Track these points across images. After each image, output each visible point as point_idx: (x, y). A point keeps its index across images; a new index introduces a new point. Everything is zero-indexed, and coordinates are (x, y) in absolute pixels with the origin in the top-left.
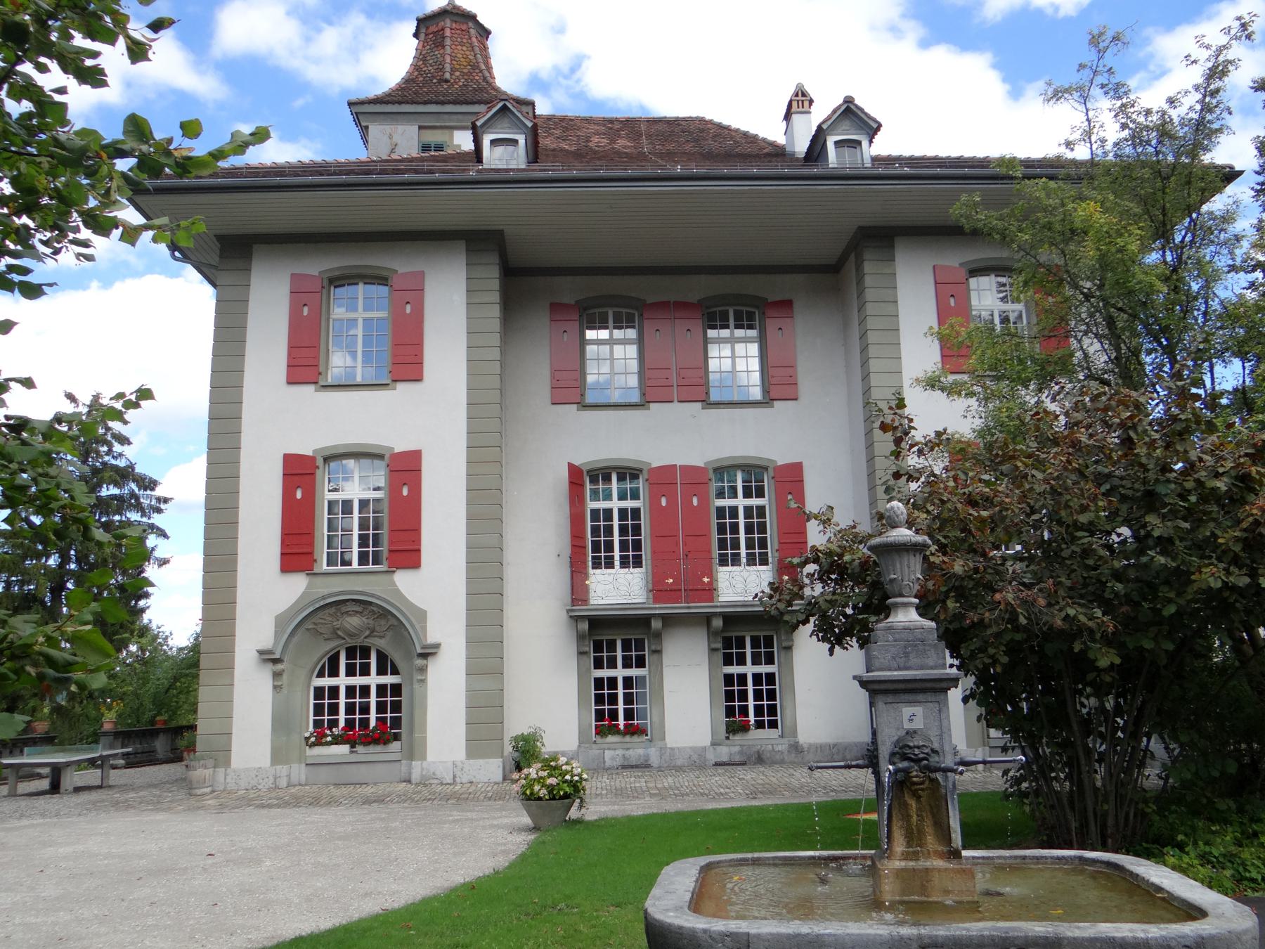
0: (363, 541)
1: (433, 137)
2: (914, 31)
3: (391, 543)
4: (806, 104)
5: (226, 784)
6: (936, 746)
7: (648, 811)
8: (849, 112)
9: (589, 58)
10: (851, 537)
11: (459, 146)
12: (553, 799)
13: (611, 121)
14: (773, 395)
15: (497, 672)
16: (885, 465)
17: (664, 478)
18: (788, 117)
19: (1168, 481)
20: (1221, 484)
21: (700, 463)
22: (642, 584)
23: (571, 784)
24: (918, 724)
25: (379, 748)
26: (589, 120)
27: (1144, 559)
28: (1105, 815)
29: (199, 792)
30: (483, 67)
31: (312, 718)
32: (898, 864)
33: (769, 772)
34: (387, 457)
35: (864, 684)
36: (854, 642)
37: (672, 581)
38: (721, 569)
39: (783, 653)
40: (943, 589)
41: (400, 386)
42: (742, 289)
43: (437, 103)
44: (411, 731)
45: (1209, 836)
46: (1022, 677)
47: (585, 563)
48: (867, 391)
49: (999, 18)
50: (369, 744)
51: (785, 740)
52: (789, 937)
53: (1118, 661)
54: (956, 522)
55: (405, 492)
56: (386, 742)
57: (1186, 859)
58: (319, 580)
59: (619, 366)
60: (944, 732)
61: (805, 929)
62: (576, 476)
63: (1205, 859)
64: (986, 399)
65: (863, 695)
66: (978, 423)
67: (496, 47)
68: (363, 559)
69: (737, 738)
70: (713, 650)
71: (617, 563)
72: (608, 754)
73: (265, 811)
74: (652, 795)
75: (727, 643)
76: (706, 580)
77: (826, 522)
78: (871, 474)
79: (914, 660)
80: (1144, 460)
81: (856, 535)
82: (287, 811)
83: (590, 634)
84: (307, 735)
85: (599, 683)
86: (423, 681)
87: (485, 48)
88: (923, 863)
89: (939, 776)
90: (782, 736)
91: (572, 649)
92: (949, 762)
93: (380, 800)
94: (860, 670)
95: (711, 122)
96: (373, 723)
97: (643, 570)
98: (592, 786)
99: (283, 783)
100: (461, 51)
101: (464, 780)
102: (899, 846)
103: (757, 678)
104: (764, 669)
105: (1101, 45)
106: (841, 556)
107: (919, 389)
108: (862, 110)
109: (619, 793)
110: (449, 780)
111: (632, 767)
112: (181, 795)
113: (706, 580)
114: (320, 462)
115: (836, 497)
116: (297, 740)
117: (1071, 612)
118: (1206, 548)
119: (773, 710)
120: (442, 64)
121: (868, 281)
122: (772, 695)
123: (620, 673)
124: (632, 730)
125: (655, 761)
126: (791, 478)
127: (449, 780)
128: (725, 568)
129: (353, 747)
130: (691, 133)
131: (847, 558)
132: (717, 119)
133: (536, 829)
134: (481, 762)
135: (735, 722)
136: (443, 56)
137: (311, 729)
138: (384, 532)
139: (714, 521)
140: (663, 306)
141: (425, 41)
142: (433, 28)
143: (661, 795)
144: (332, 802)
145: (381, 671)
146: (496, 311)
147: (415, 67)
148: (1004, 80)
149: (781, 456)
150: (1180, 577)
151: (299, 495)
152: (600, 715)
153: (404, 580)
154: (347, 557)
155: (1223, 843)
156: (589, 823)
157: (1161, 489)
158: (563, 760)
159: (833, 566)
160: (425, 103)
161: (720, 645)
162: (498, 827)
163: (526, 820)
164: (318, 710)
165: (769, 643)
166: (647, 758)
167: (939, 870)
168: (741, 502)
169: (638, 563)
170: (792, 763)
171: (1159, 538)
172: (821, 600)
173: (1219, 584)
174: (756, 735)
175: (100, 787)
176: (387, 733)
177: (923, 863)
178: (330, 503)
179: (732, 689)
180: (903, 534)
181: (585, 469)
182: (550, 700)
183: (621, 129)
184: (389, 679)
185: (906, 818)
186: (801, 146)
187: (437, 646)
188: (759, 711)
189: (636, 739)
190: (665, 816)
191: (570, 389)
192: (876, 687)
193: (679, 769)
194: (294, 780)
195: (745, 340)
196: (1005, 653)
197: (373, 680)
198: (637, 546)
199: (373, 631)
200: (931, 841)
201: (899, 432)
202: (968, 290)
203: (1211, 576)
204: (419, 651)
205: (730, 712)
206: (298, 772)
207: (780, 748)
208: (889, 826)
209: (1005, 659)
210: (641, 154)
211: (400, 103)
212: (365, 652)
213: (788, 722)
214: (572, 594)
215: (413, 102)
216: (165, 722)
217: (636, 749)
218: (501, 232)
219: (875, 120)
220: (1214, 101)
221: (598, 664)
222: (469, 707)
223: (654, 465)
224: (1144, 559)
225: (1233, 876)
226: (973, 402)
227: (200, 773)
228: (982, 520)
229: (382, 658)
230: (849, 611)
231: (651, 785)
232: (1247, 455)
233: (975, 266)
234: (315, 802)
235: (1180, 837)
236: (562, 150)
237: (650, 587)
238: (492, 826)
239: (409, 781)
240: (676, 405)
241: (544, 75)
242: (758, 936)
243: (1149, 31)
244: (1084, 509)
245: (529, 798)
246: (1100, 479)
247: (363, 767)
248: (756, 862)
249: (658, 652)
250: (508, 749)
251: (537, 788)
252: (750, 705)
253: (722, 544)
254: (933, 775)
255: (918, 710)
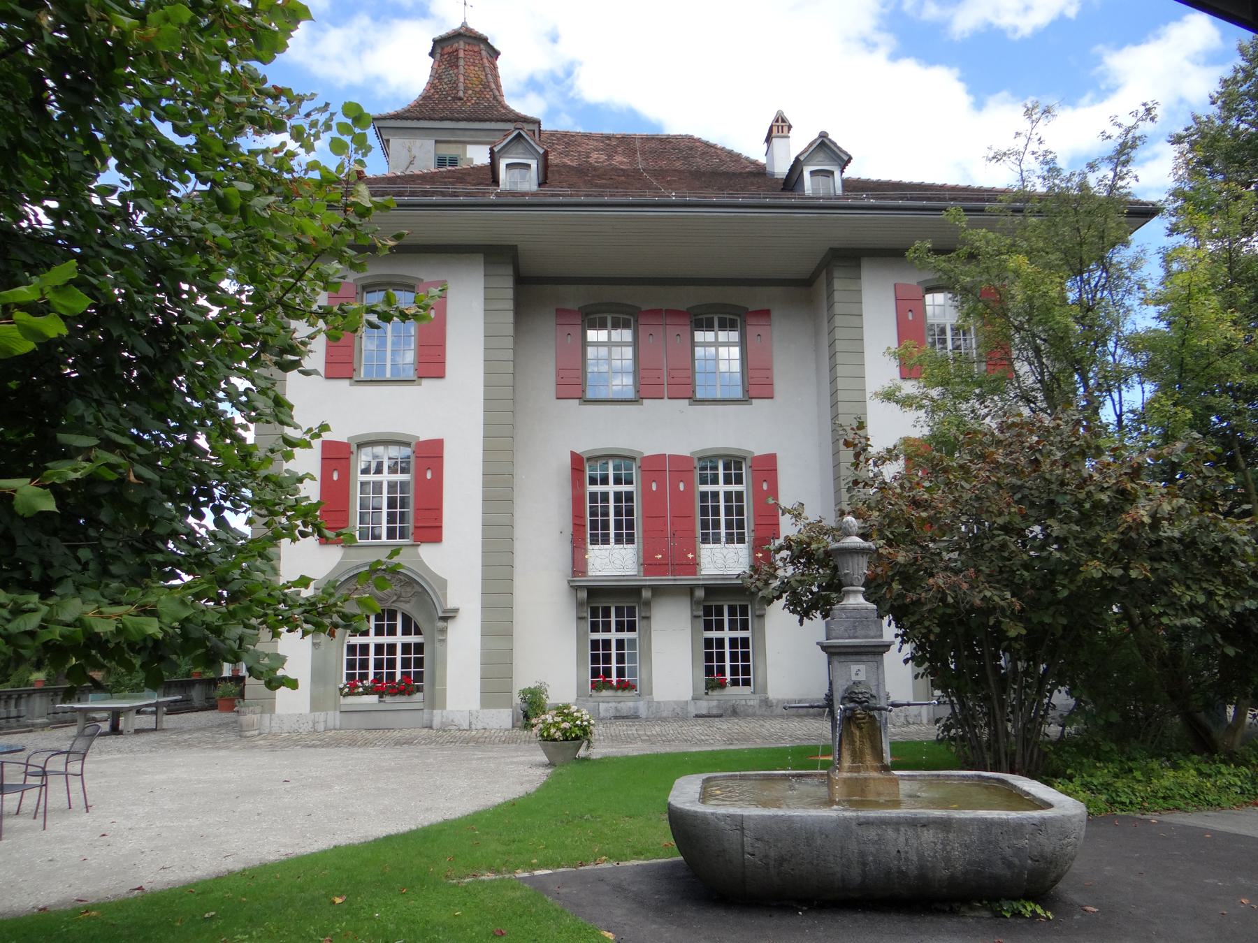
0: (391, 518)
1: (449, 151)
2: (887, 42)
3: (416, 520)
4: (786, 129)
5: (271, 727)
6: (874, 692)
7: (642, 753)
8: (824, 145)
9: (581, 64)
10: (819, 529)
11: (471, 160)
12: (567, 740)
13: (609, 138)
14: (752, 394)
15: (508, 634)
16: (847, 473)
17: (654, 466)
18: (769, 139)
19: (1065, 493)
20: (1104, 497)
21: (685, 451)
22: (635, 559)
23: (581, 727)
24: (862, 677)
25: (404, 698)
26: (588, 136)
27: (1044, 554)
28: (1013, 754)
29: (248, 734)
30: (493, 86)
31: (345, 671)
32: (846, 775)
33: (742, 723)
34: (413, 444)
35: (824, 648)
36: (818, 614)
37: (656, 549)
38: (703, 546)
39: (756, 620)
40: (890, 573)
41: (425, 382)
42: (726, 298)
43: (451, 120)
44: (433, 684)
45: (1093, 771)
46: (952, 648)
47: (584, 540)
48: (835, 417)
49: (967, 35)
50: (396, 694)
51: (757, 696)
52: (770, 817)
53: (1024, 632)
54: (897, 521)
55: (429, 476)
56: (410, 693)
57: (1071, 786)
58: (352, 551)
59: (617, 364)
60: (880, 683)
61: (780, 812)
62: (578, 462)
63: (1086, 786)
64: (933, 412)
65: (824, 655)
66: (926, 431)
67: (503, 65)
68: (391, 534)
69: (716, 694)
70: (695, 617)
71: (612, 540)
72: (602, 706)
73: (312, 750)
74: (643, 741)
75: (708, 611)
76: (690, 556)
77: (798, 516)
78: (837, 478)
79: (859, 632)
80: (1048, 476)
81: (822, 528)
82: (331, 750)
83: (588, 602)
84: (341, 686)
85: (595, 644)
86: (444, 641)
87: (495, 68)
88: (863, 774)
89: (875, 713)
90: (754, 693)
91: (572, 614)
92: (883, 704)
93: (409, 742)
94: (822, 638)
95: (699, 140)
96: (398, 677)
97: (635, 546)
98: (598, 731)
99: (321, 727)
100: (473, 71)
101: (479, 727)
102: (847, 762)
103: (733, 642)
104: (739, 634)
105: (1034, 117)
106: (809, 544)
107: (877, 401)
108: (835, 144)
109: (615, 739)
110: (466, 726)
111: (623, 718)
112: (232, 737)
113: (690, 556)
114: (354, 448)
115: (806, 493)
116: (332, 690)
117: (988, 594)
118: (1091, 546)
119: (746, 670)
120: (456, 82)
121: (837, 296)
122: (746, 657)
123: (613, 636)
124: (624, 686)
125: (643, 712)
126: (767, 467)
127: (466, 726)
128: (707, 546)
129: (381, 697)
130: (681, 151)
131: (814, 546)
132: (705, 138)
133: (551, 764)
134: (494, 711)
135: (713, 679)
136: (457, 75)
137: (344, 681)
138: (410, 510)
139: (698, 504)
140: (656, 313)
141: (441, 61)
142: (448, 49)
143: (650, 740)
144: (366, 744)
145: (406, 632)
146: (509, 317)
147: (431, 85)
148: (969, 92)
149: (755, 444)
150: (1074, 568)
151: (335, 477)
152: (595, 673)
153: (428, 554)
154: (377, 532)
155: (1102, 775)
156: (594, 760)
157: (1060, 500)
158: (574, 708)
159: (802, 552)
160: (442, 119)
161: (701, 613)
162: (518, 763)
163: (545, 759)
164: (351, 665)
165: (744, 611)
166: (636, 709)
167: (874, 779)
168: (721, 488)
169: (630, 540)
170: (763, 716)
171: (1057, 537)
172: (792, 580)
173: (1100, 575)
174: (731, 691)
175: (156, 730)
176: (408, 687)
177: (863, 774)
178: (362, 484)
179: (711, 652)
180: (855, 541)
181: (585, 457)
182: (553, 658)
183: (617, 146)
184: (412, 639)
185: (852, 742)
186: (781, 168)
187: (456, 610)
188: (734, 670)
189: (626, 693)
190: (658, 756)
191: (574, 385)
192: (833, 650)
193: (664, 720)
194: (330, 725)
195: (728, 344)
196: (938, 625)
197: (399, 639)
198: (630, 525)
199: (399, 596)
200: (869, 759)
201: (860, 450)
202: (924, 305)
203: (1095, 569)
204: (440, 614)
205: (709, 671)
206: (334, 718)
207: (752, 703)
208: (840, 750)
209: (937, 630)
210: (636, 171)
211: (418, 119)
212: (392, 615)
213: (760, 680)
214: (573, 566)
215: (431, 119)
216: (200, 674)
217: (627, 702)
218: (514, 248)
219: (846, 153)
220: (1125, 170)
221: (595, 628)
222: (484, 664)
223: (646, 454)
224: (1044, 554)
225: (1107, 801)
226: (922, 413)
227: (249, 717)
228: (924, 520)
229: (407, 620)
230: (815, 589)
231: (641, 732)
232: (1126, 474)
233: (928, 285)
234: (353, 743)
235: (1069, 771)
236: (565, 166)
237: (641, 561)
238: (512, 763)
239: (431, 727)
240: (666, 401)
241: (540, 77)
242: (749, 817)
243: (1099, 48)
244: (1001, 514)
245: (547, 739)
246: (1014, 489)
247: (382, 714)
248: (742, 778)
249: (648, 618)
250: (517, 700)
251: (553, 730)
252: (726, 665)
253: (705, 525)
254: (871, 713)
255: (862, 667)
